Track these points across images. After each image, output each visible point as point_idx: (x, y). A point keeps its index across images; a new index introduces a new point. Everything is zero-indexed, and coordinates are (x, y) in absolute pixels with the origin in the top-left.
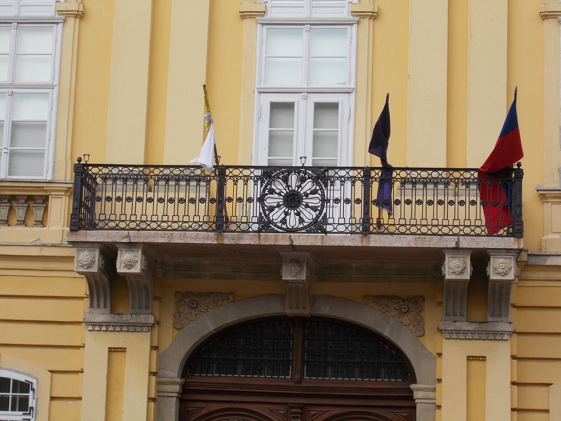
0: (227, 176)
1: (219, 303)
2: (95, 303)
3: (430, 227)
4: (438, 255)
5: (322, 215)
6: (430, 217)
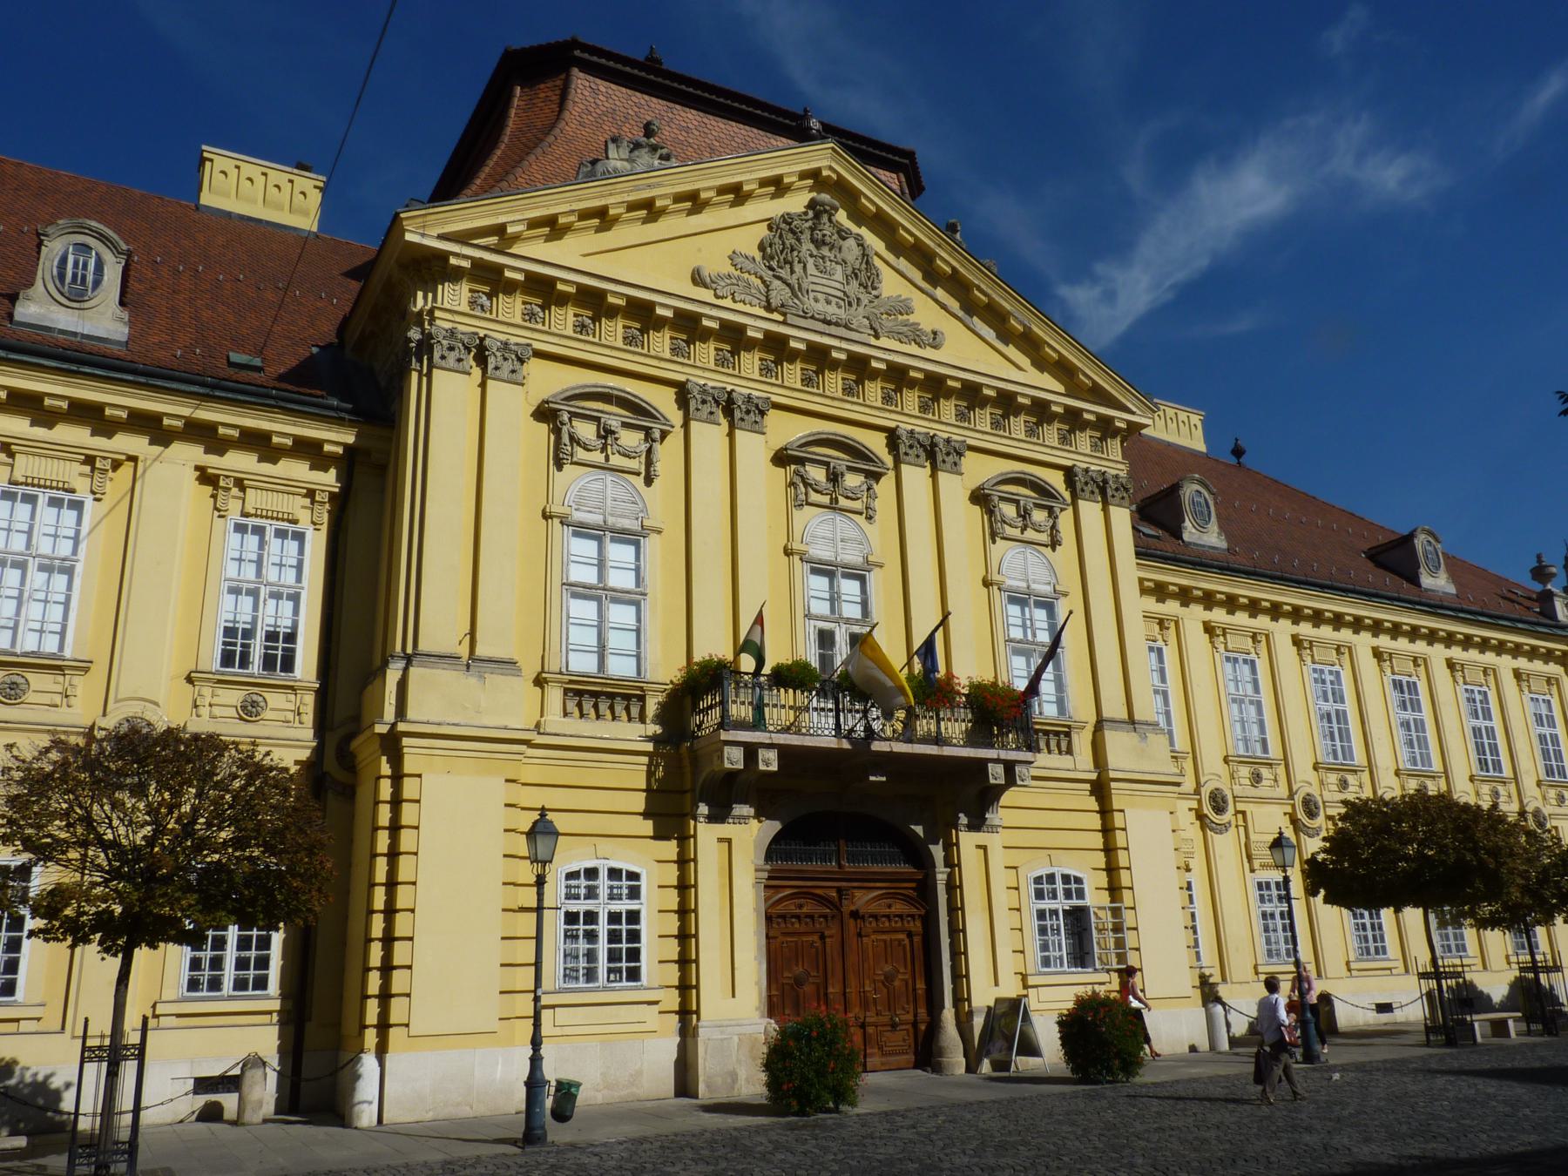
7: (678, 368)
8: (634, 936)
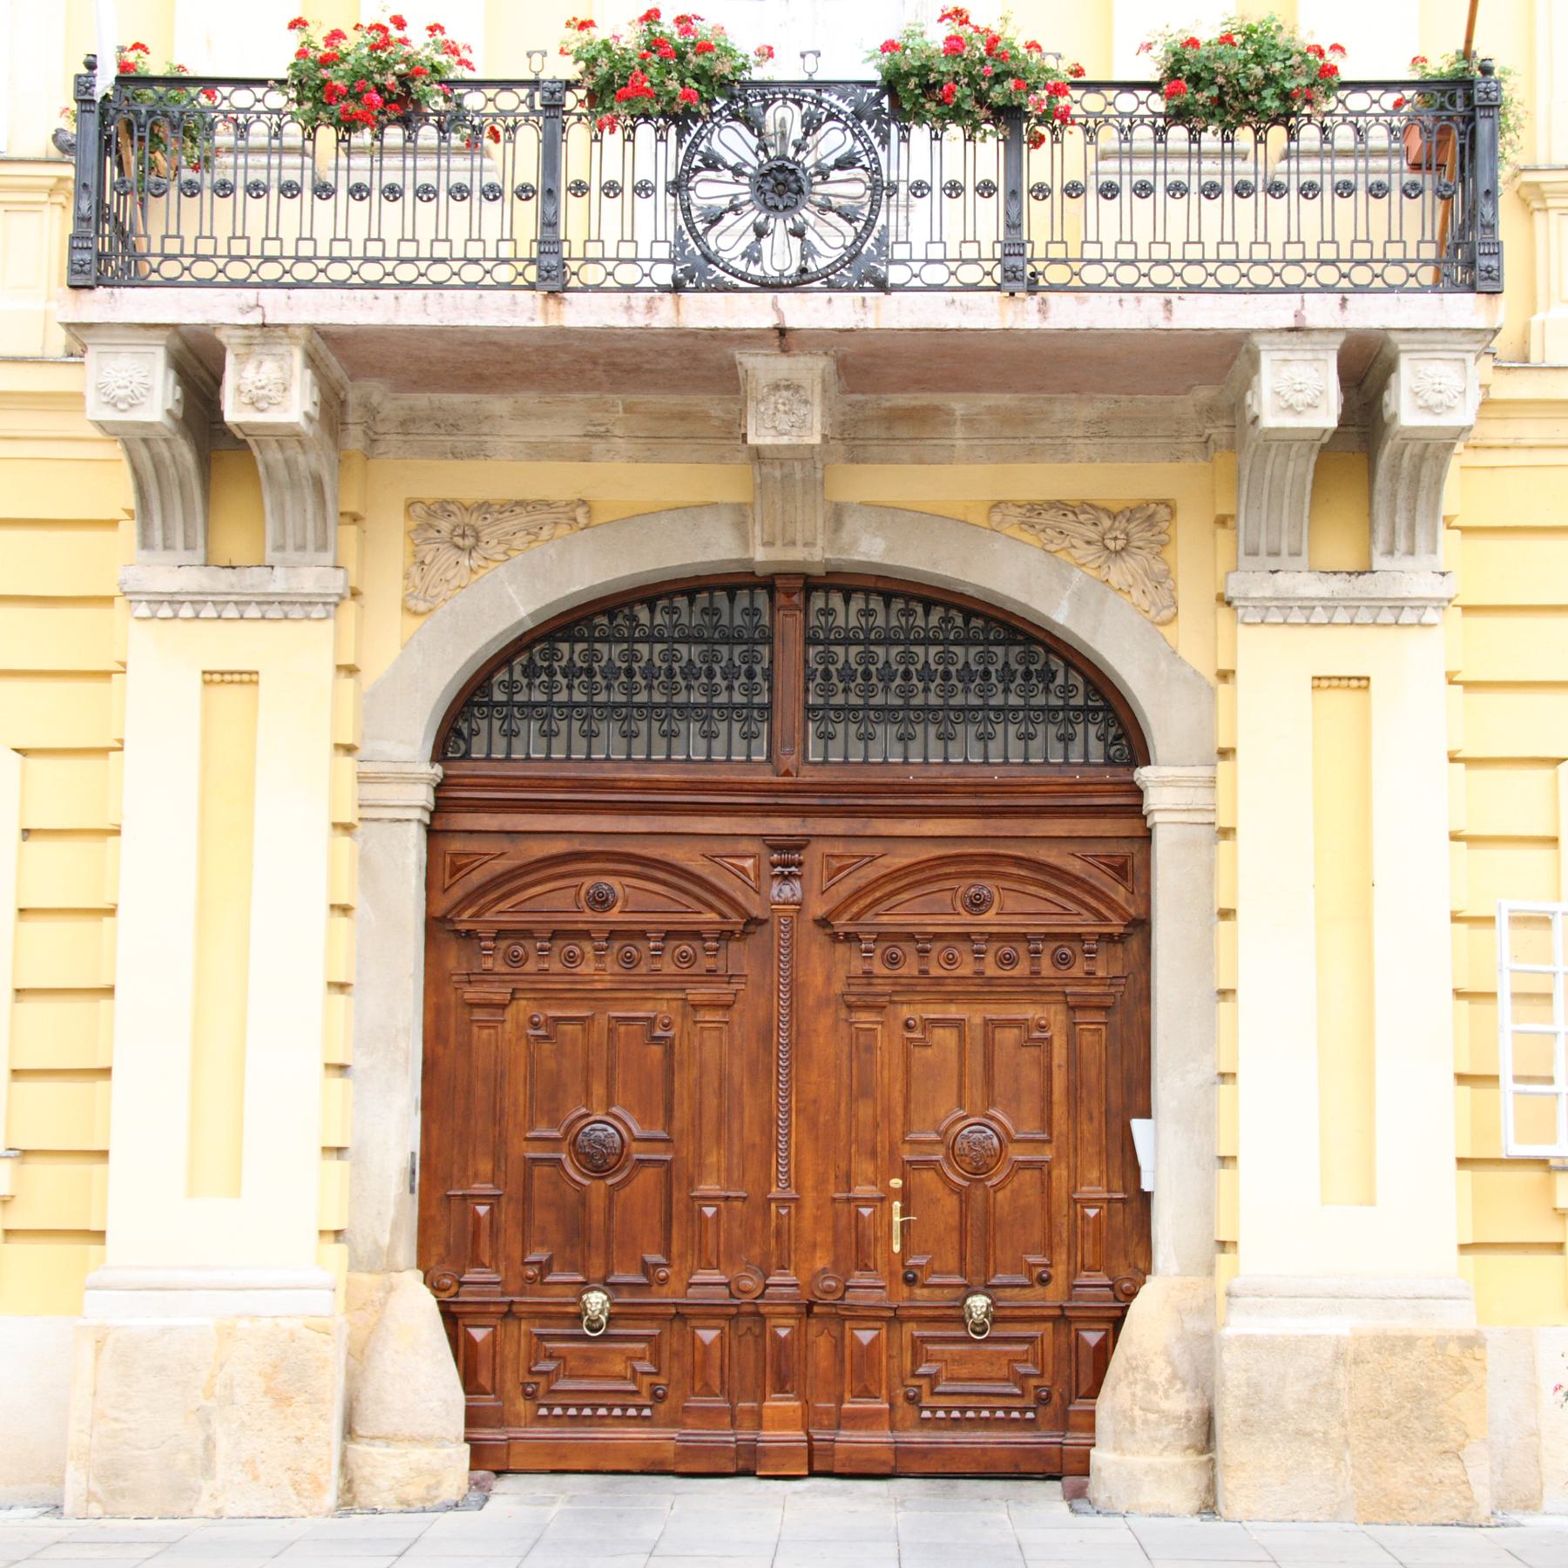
0: (569, 113)
1: (545, 534)
2: (157, 535)
3: (1211, 267)
4: (1229, 357)
5: (875, 233)
6: (1211, 238)
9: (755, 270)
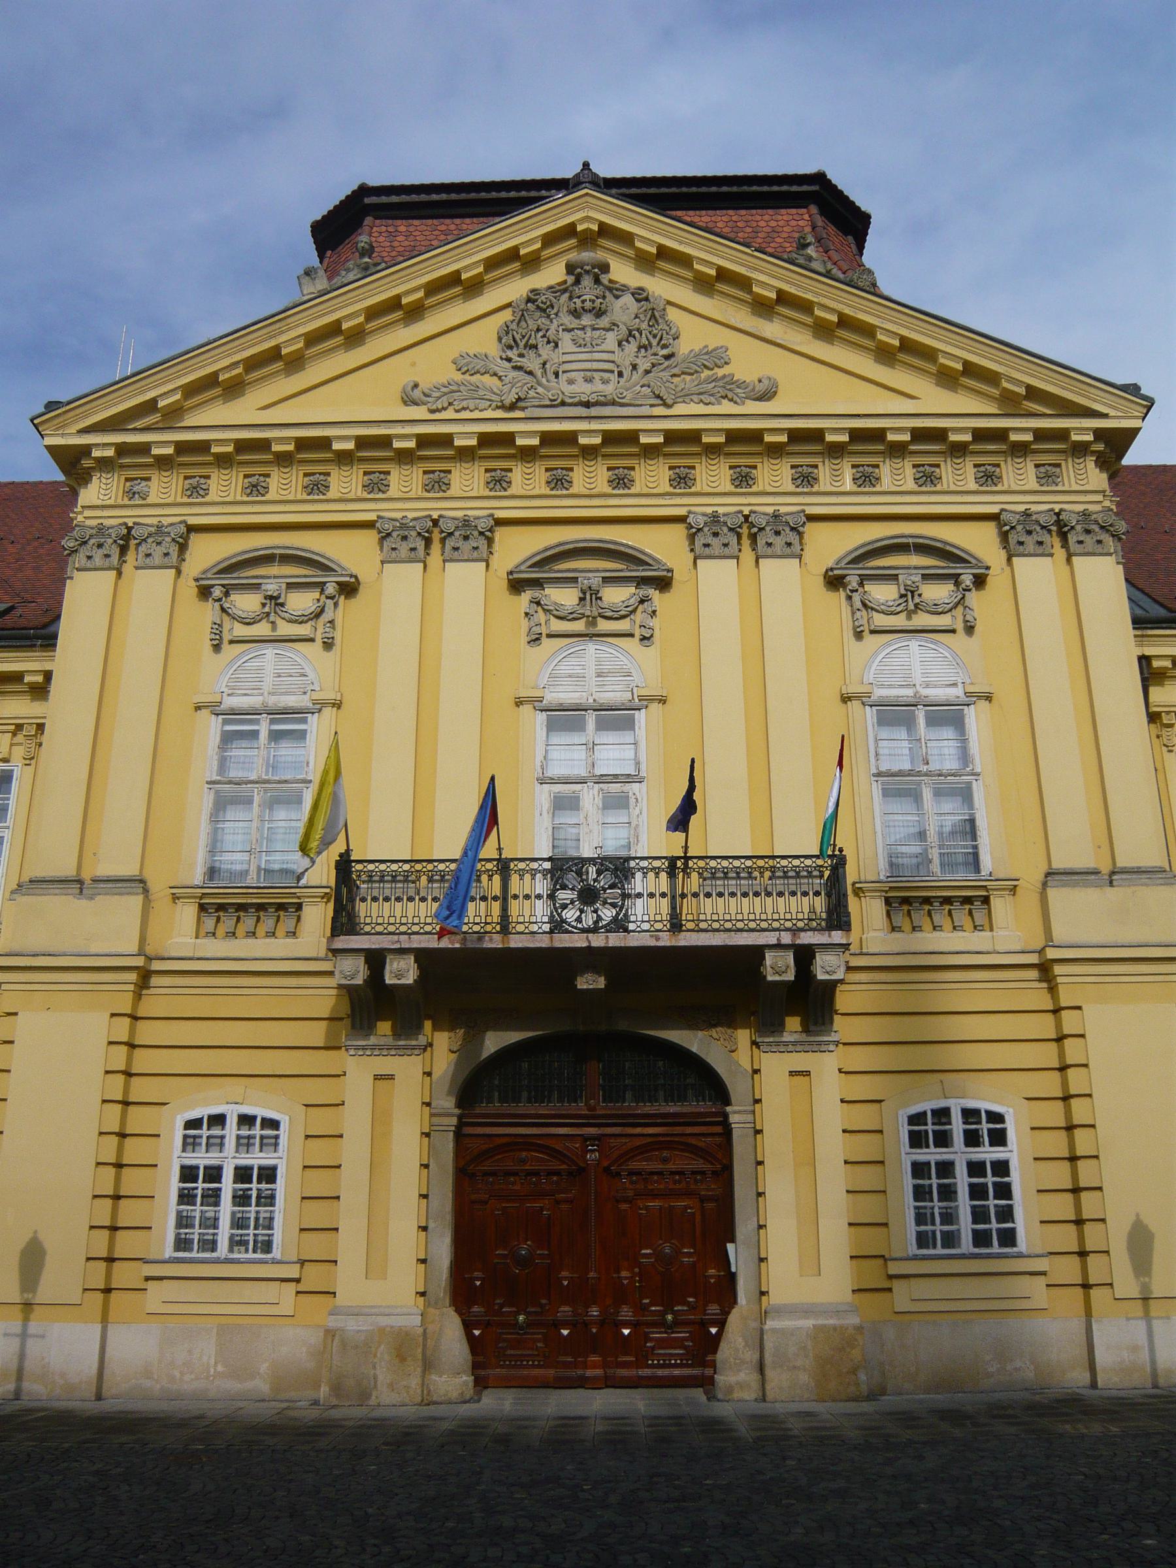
6: (745, 911)
7: (678, 501)
8: (1004, 1191)
9: (579, 926)
